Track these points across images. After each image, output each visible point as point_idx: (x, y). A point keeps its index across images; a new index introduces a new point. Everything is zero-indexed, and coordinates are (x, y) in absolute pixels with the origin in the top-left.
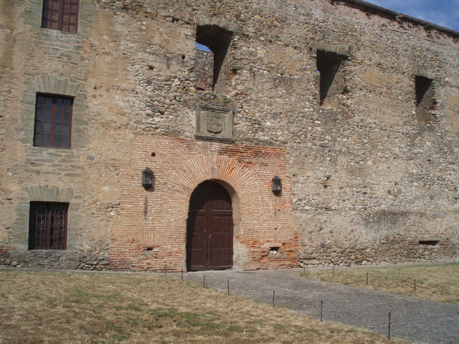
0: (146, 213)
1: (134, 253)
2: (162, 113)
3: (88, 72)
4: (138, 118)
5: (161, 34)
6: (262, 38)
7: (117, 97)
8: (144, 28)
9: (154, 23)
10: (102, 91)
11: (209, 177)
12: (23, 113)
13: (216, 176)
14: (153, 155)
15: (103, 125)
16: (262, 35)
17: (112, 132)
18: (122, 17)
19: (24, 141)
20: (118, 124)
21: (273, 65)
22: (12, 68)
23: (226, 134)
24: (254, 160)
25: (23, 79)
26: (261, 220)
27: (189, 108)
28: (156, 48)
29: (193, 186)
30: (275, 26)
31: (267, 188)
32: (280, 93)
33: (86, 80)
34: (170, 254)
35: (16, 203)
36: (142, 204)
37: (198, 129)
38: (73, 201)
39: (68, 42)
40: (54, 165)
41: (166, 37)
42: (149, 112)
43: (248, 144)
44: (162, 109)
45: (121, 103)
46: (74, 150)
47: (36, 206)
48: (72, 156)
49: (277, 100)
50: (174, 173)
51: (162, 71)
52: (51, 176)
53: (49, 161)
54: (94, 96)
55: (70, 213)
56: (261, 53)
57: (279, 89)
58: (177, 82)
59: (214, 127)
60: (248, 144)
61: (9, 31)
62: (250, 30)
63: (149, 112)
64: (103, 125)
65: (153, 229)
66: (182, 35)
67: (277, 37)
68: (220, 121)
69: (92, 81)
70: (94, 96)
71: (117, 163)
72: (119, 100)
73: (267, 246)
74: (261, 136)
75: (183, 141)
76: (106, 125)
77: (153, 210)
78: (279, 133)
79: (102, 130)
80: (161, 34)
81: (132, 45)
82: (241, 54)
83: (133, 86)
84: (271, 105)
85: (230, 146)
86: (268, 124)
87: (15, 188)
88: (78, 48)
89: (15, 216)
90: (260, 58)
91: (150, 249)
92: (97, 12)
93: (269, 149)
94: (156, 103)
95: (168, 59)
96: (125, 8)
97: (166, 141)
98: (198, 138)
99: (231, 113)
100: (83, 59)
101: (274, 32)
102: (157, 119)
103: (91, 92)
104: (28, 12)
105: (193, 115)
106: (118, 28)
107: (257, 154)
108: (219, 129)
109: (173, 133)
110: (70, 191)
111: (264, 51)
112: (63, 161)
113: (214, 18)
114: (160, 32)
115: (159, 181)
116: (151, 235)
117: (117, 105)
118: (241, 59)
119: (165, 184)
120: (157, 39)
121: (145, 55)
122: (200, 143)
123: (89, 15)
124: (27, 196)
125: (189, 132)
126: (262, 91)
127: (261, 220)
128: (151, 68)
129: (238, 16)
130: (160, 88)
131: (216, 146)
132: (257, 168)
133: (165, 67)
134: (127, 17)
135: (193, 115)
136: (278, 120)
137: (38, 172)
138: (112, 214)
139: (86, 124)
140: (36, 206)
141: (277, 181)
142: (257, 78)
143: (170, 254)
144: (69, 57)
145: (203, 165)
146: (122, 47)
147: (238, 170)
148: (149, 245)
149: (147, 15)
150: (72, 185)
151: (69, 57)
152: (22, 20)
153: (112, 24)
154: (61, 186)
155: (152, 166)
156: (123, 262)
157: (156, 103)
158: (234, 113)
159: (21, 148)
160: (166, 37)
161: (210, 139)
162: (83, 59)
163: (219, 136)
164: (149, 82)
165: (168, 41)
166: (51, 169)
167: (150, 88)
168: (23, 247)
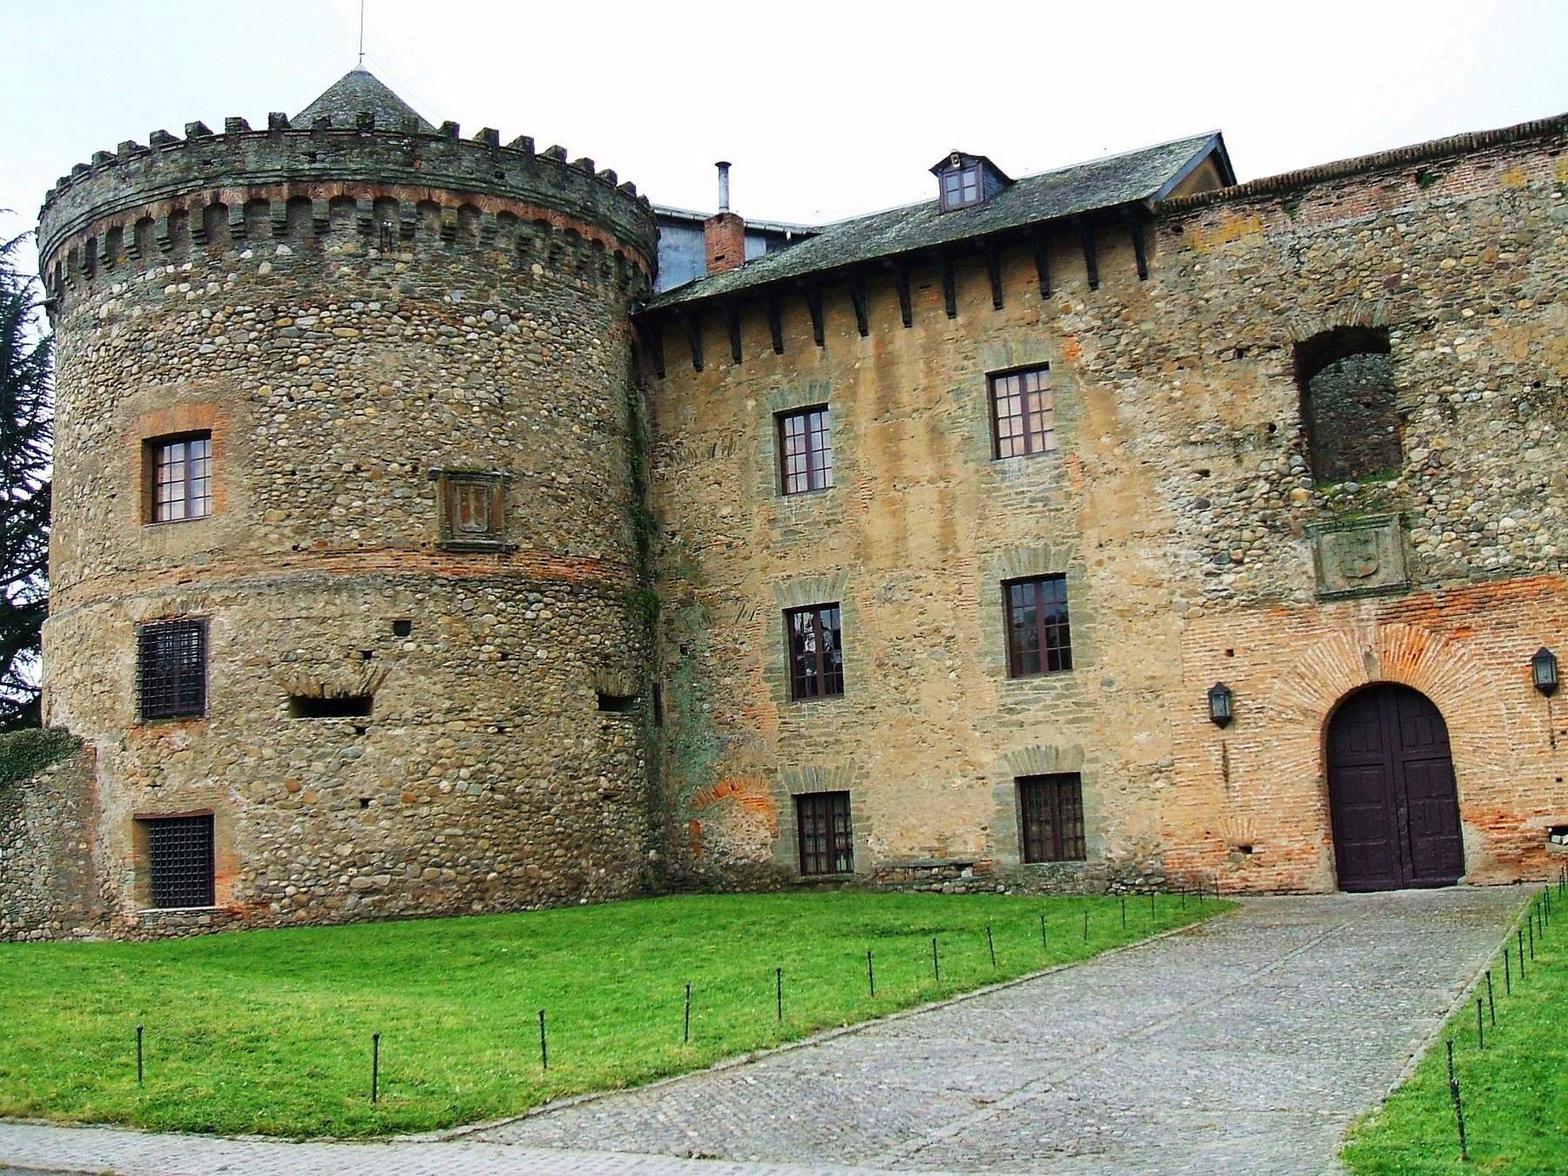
0: (1226, 775)
1: (1210, 858)
2: (1240, 562)
3: (1081, 520)
4: (1189, 585)
5: (1214, 393)
6: (1468, 313)
7: (1142, 553)
8: (1177, 394)
9: (1196, 378)
10: (1114, 550)
11: (1361, 680)
12: (988, 634)
13: (1377, 676)
14: (1230, 653)
15: (1121, 614)
16: (1466, 303)
17: (1141, 625)
18: (1131, 388)
19: (992, 673)
20: (1151, 607)
21: (1507, 371)
22: (958, 550)
23: (1390, 574)
24: (1474, 620)
25: (976, 563)
26: (1512, 762)
27: (1296, 536)
28: (1207, 427)
29: (1325, 706)
30: (1504, 266)
31: (1519, 684)
32: (1536, 435)
33: (1080, 536)
34: (1288, 857)
35: (992, 782)
36: (1216, 757)
37: (1320, 579)
38: (1085, 769)
39: (1039, 472)
40: (1046, 708)
41: (1226, 396)
42: (1211, 567)
43: (1454, 584)
44: (1238, 554)
45: (1150, 564)
46: (1076, 674)
47: (1026, 784)
48: (1075, 686)
49: (1529, 455)
50: (1278, 684)
51: (1226, 471)
52: (1044, 725)
53: (1036, 701)
54: (1100, 563)
55: (1086, 791)
56: (1466, 347)
57: (1532, 425)
58: (1263, 486)
59: (1359, 564)
60: (1454, 584)
61: (942, 484)
62: (1431, 304)
63: (1211, 567)
64: (1121, 614)
65: (1245, 807)
66: (1263, 380)
67: (1513, 292)
68: (1371, 549)
69: (1092, 534)
70: (1100, 563)
71: (1157, 685)
72: (1146, 558)
73: (1536, 824)
74: (1489, 557)
75: (1290, 612)
76: (1127, 614)
77: (1239, 768)
78: (1541, 538)
79: (1122, 624)
80: (1214, 393)
81: (1159, 438)
82: (1414, 371)
83: (1170, 523)
84: (1511, 473)
85: (1403, 596)
86: (1507, 522)
87: (987, 757)
88: (1061, 476)
89: (993, 806)
90: (1470, 366)
91: (1247, 849)
92: (1082, 396)
93: (1517, 586)
94: (1222, 545)
95: (1237, 443)
96: (1136, 366)
97: (1253, 620)
98: (1323, 598)
99: (1396, 521)
100: (1069, 496)
101: (1501, 282)
102: (1228, 578)
103: (1092, 555)
104: (967, 440)
105: (1304, 552)
106: (1127, 412)
107: (1481, 605)
108: (1372, 566)
109: (1266, 601)
110: (1079, 751)
111: (1477, 342)
112: (1060, 697)
113: (1331, 314)
114: (1211, 397)
115: (1245, 703)
116: (1242, 820)
117: (1143, 569)
118: (1414, 384)
119: (1261, 709)
120: (1207, 409)
121: (1187, 451)
122: (1330, 607)
123: (1070, 407)
124: (1007, 768)
125: (1303, 592)
126: (1480, 445)
127: (1512, 762)
128: (1206, 473)
129: (1391, 284)
130: (1225, 512)
131: (1369, 607)
132: (1485, 636)
133: (1231, 462)
134: (1142, 383)
135: (1304, 552)
136: (1535, 505)
137: (1021, 725)
138: (1159, 784)
139: (1091, 618)
140: (1026, 784)
141: (1543, 658)
142: (1462, 419)
143: (1288, 857)
144: (1045, 501)
145: (1337, 657)
146: (1140, 450)
147: (1432, 649)
148: (1243, 837)
149: (1182, 363)
150: (1080, 740)
151: (1045, 501)
152: (961, 456)
153: (1113, 410)
154: (1061, 743)
155: (1228, 678)
156: (1196, 878)
157: (1222, 545)
158: (1403, 518)
159: (991, 688)
160: (1226, 396)
161: (1353, 595)
162: (1069, 496)
163: (1374, 583)
164: (1203, 505)
165: (1231, 405)
166: (1041, 715)
167: (1207, 515)
168: (1011, 859)
